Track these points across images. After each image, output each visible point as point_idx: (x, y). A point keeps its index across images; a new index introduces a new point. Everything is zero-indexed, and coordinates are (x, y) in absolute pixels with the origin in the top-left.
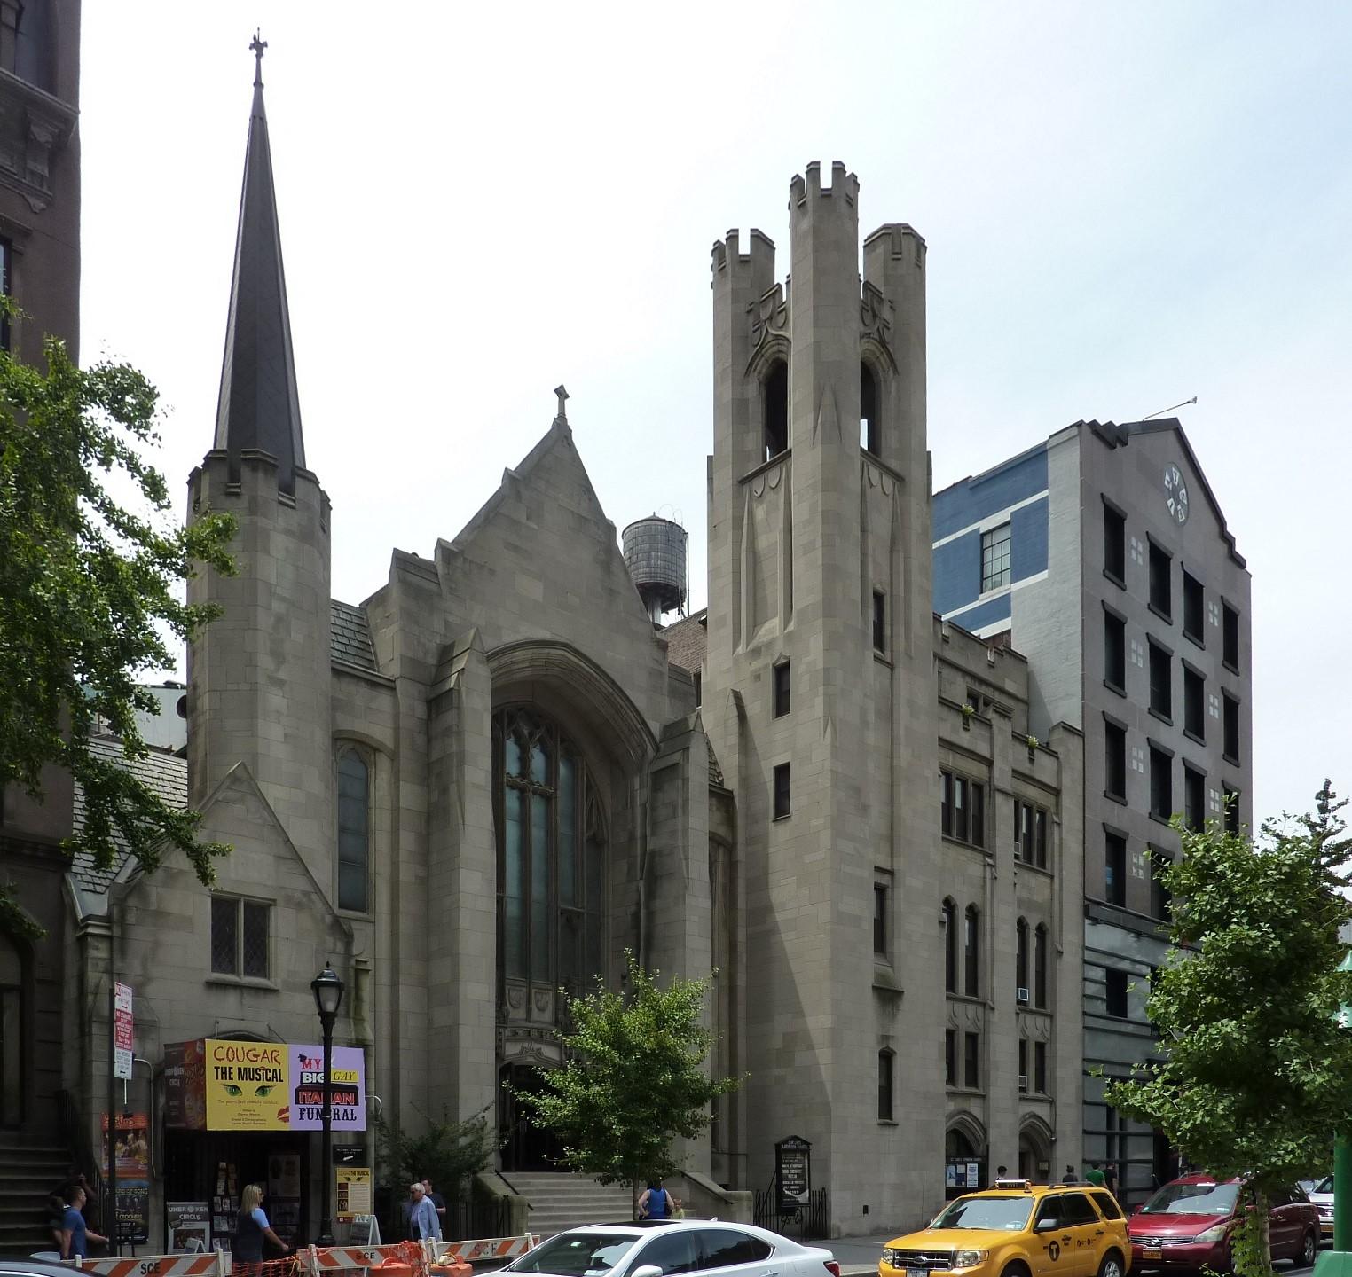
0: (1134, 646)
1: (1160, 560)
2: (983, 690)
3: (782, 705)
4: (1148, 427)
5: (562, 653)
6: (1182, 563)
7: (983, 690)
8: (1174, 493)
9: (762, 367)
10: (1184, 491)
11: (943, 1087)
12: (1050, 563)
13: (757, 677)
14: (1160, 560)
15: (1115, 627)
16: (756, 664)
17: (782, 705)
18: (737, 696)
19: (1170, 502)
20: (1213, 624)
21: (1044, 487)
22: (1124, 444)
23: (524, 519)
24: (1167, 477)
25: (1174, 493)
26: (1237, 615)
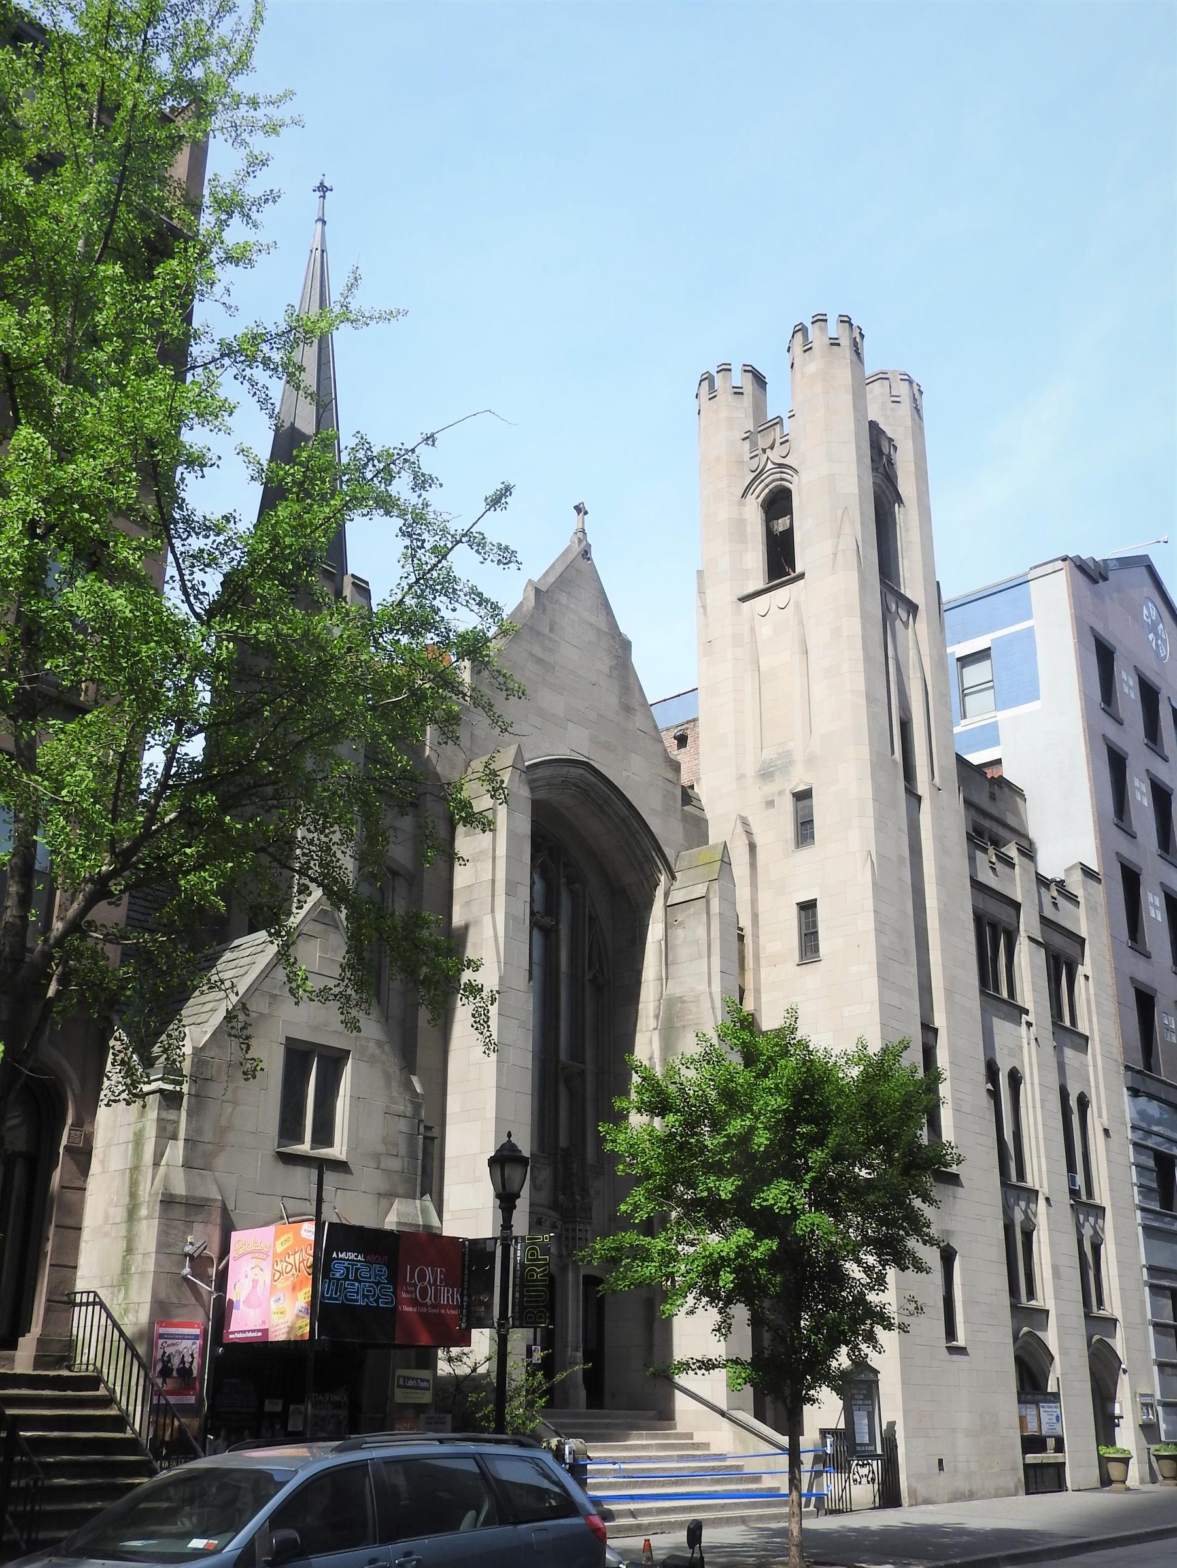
0: (1137, 783)
1: (1149, 694)
2: (987, 824)
3: (804, 830)
4: (1126, 563)
5: (581, 771)
6: (744, 599)
7: (987, 824)
8: (1153, 628)
9: (761, 492)
10: (1161, 626)
11: (943, 1342)
12: (1042, 693)
13: (770, 804)
14: (1149, 694)
15: (1117, 763)
16: (771, 788)
17: (804, 830)
18: (745, 823)
19: (1151, 636)
20: (1141, 803)
21: (1030, 617)
22: (1105, 579)
23: (546, 630)
24: (1145, 612)
25: (1153, 628)
26: (1170, 795)
